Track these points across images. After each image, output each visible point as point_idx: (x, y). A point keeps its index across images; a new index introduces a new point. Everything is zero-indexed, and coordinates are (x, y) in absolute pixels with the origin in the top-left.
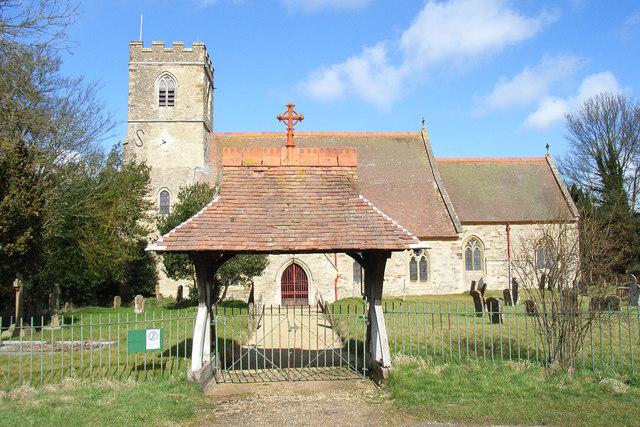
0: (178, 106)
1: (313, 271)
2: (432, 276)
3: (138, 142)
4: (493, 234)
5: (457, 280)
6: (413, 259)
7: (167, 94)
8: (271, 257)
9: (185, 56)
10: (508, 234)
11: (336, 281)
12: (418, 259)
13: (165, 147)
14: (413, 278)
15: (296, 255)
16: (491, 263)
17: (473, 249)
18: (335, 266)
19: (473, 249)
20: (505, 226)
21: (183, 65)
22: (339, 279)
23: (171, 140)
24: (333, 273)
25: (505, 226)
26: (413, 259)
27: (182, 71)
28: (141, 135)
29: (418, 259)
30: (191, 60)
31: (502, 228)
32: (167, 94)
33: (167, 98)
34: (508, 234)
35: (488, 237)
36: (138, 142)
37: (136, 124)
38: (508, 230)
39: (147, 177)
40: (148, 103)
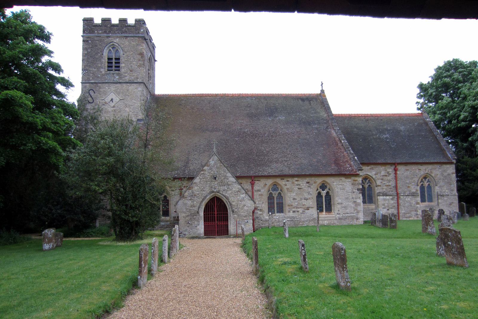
0: (123, 70)
1: (233, 203)
2: (336, 208)
3: (90, 99)
4: (383, 173)
5: (358, 212)
6: (319, 194)
7: (114, 61)
8: (238, 232)
9: (128, 29)
10: (396, 174)
11: (253, 212)
12: (324, 193)
13: (112, 104)
14: (320, 208)
15: (85, 82)
16: (382, 197)
17: (366, 186)
18: (252, 198)
19: (366, 186)
20: (393, 167)
21: (126, 37)
22: (256, 211)
23: (116, 99)
24: (249, 205)
25: (393, 167)
26: (319, 194)
27: (126, 42)
28: (92, 93)
29: (324, 193)
30: (133, 34)
31: (390, 169)
32: (114, 61)
33: (114, 64)
34: (396, 174)
35: (378, 176)
36: (90, 99)
37: (88, 85)
38: (396, 170)
39: (142, 240)
40: (99, 68)
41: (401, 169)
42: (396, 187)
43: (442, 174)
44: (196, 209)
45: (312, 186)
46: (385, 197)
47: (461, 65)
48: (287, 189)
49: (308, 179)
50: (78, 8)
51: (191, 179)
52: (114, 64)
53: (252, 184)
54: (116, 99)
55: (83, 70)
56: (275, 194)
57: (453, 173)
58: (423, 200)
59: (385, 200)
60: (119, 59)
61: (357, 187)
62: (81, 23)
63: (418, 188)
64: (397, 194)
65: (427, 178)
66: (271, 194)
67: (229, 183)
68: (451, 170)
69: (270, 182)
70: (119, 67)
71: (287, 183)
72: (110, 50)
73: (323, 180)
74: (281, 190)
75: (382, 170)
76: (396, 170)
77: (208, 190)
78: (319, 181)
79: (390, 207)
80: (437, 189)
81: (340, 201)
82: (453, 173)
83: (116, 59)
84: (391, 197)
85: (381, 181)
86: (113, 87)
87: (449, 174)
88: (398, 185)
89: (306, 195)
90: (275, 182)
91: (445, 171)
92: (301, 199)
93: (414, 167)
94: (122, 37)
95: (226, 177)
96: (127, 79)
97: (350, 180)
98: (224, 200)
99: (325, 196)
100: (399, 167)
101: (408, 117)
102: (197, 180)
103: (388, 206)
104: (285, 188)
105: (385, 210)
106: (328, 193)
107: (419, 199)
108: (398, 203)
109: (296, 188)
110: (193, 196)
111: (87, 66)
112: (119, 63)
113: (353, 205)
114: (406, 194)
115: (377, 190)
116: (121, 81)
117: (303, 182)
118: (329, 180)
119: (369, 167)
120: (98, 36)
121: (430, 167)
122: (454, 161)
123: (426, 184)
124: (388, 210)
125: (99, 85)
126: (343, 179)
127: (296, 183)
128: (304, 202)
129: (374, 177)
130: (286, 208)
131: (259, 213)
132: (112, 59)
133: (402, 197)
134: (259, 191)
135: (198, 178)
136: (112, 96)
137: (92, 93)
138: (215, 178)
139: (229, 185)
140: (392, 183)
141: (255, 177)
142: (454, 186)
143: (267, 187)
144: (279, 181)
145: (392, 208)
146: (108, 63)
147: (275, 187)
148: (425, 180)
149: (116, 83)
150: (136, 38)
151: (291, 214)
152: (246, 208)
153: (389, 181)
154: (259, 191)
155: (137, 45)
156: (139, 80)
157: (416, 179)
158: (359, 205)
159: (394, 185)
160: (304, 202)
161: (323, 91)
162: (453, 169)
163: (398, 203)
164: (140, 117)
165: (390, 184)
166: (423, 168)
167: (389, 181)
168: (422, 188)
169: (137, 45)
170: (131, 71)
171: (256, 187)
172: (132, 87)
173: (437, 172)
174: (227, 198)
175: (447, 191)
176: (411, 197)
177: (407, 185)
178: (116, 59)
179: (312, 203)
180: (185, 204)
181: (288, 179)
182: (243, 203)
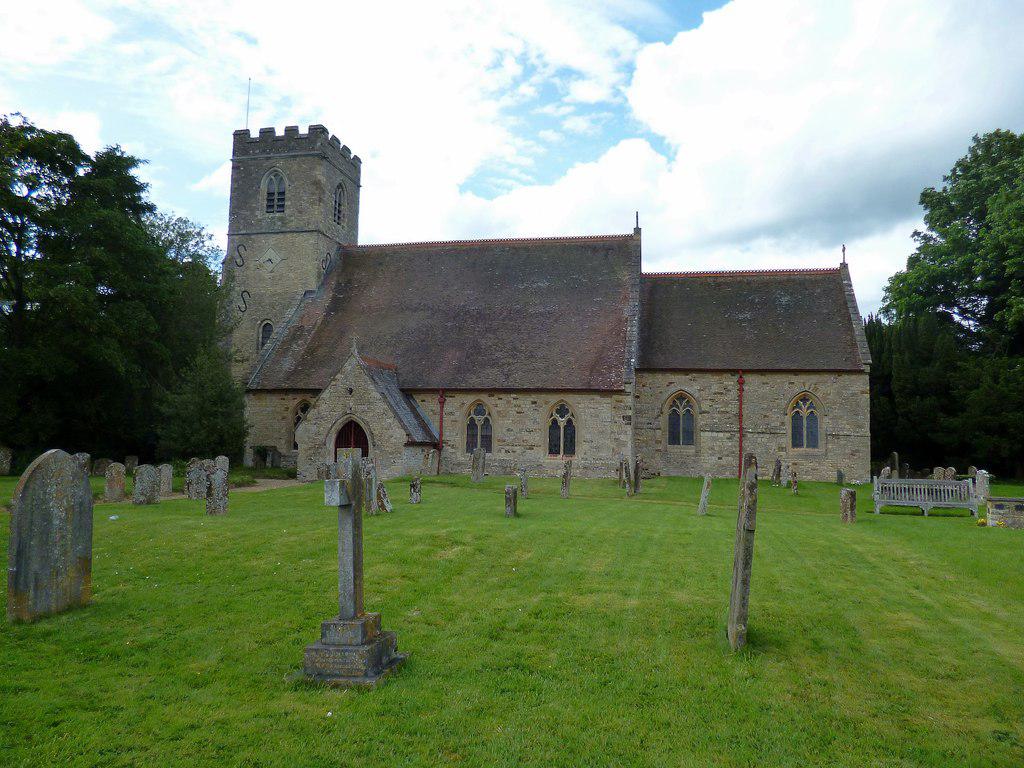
2: (581, 448)
4: (715, 388)
7: (276, 196)
12: (562, 422)
26: (555, 422)
28: (241, 249)
29: (562, 422)
31: (730, 382)
32: (276, 196)
34: (741, 390)
37: (237, 237)
38: (741, 383)
40: (253, 210)
41: (753, 382)
42: (740, 416)
43: (839, 394)
44: (321, 438)
45: (541, 410)
46: (715, 434)
47: (1001, 167)
48: (499, 412)
49: (534, 397)
50: (81, 148)
51: (317, 392)
52: (276, 201)
53: (442, 403)
54: (276, 259)
55: (232, 213)
56: (479, 420)
57: (863, 392)
58: (795, 445)
59: (715, 439)
60: (283, 193)
61: (622, 413)
62: (231, 140)
63: (788, 419)
64: (741, 429)
65: (808, 400)
66: (472, 420)
67: (371, 400)
68: (860, 385)
69: (470, 399)
70: (283, 206)
71: (498, 402)
72: (271, 179)
73: (477, 398)
74: (489, 414)
75: (714, 383)
76: (741, 383)
77: (339, 410)
78: (554, 399)
79: (726, 453)
80: (825, 424)
81: (588, 436)
82: (863, 392)
83: (279, 193)
84: (728, 435)
85: (709, 403)
86: (273, 239)
87: (853, 395)
88: (745, 412)
89: (530, 425)
90: (479, 400)
91: (845, 388)
92: (521, 430)
93: (779, 379)
94: (286, 157)
95: (366, 390)
96: (293, 225)
97: (608, 400)
98: (362, 425)
99: (565, 427)
100: (748, 378)
101: (807, 277)
102: (325, 395)
103: (721, 452)
104: (494, 412)
105: (714, 459)
106: (569, 422)
107: (787, 441)
108: (741, 446)
109: (513, 411)
110: (320, 417)
111: (236, 207)
112: (283, 200)
113: (613, 445)
114: (759, 430)
115: (701, 421)
116: (283, 229)
117: (525, 402)
118: (570, 399)
119: (689, 377)
120: (254, 159)
121: (814, 378)
122: (867, 369)
123: (805, 412)
124: (719, 458)
125: (253, 237)
126: (597, 397)
127: (514, 402)
128: (526, 436)
129: (696, 395)
130: (495, 445)
131: (451, 450)
132: (274, 194)
133: (749, 435)
134: (452, 413)
135: (327, 391)
136: (270, 254)
137: (241, 249)
138: (351, 391)
139: (370, 403)
140: (733, 409)
141: (445, 391)
142: (865, 419)
143: (466, 406)
144: (484, 398)
145: (728, 456)
146: (268, 200)
147: (480, 409)
148: (804, 404)
149: (278, 233)
150: (309, 158)
151: (502, 456)
152: (393, 440)
153: (727, 404)
154: (452, 413)
155: (310, 169)
156: (312, 227)
157: (784, 403)
158: (624, 444)
159: (735, 410)
160: (526, 436)
161: (638, 230)
162: (864, 384)
163: (741, 446)
164: (310, 288)
165: (728, 410)
166: (798, 380)
167: (727, 404)
168: (797, 418)
169: (310, 169)
170: (300, 212)
171: (447, 408)
172: (299, 238)
173: (826, 388)
174: (367, 424)
175: (848, 427)
176: (768, 436)
177: (764, 413)
178: (279, 193)
179: (541, 438)
180: (307, 430)
181: (501, 396)
182: (390, 432)
